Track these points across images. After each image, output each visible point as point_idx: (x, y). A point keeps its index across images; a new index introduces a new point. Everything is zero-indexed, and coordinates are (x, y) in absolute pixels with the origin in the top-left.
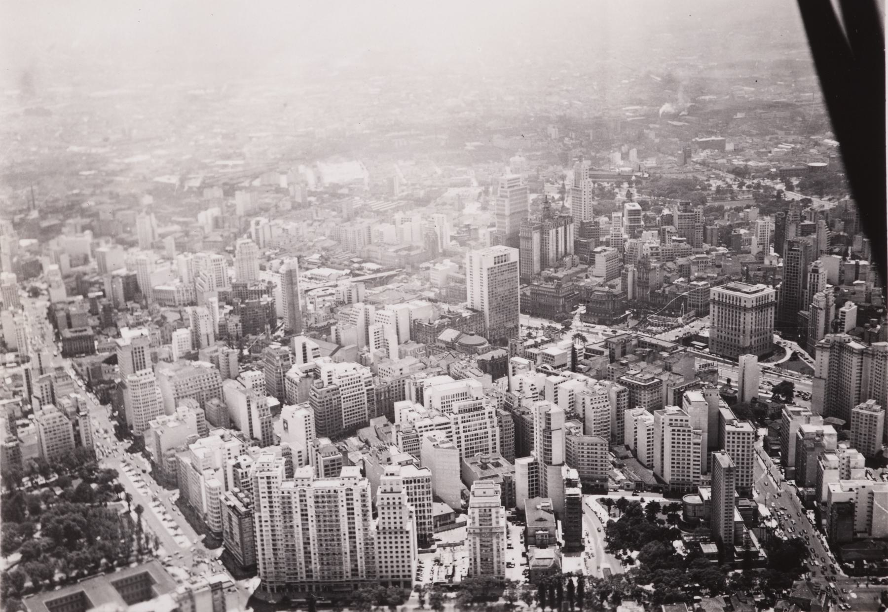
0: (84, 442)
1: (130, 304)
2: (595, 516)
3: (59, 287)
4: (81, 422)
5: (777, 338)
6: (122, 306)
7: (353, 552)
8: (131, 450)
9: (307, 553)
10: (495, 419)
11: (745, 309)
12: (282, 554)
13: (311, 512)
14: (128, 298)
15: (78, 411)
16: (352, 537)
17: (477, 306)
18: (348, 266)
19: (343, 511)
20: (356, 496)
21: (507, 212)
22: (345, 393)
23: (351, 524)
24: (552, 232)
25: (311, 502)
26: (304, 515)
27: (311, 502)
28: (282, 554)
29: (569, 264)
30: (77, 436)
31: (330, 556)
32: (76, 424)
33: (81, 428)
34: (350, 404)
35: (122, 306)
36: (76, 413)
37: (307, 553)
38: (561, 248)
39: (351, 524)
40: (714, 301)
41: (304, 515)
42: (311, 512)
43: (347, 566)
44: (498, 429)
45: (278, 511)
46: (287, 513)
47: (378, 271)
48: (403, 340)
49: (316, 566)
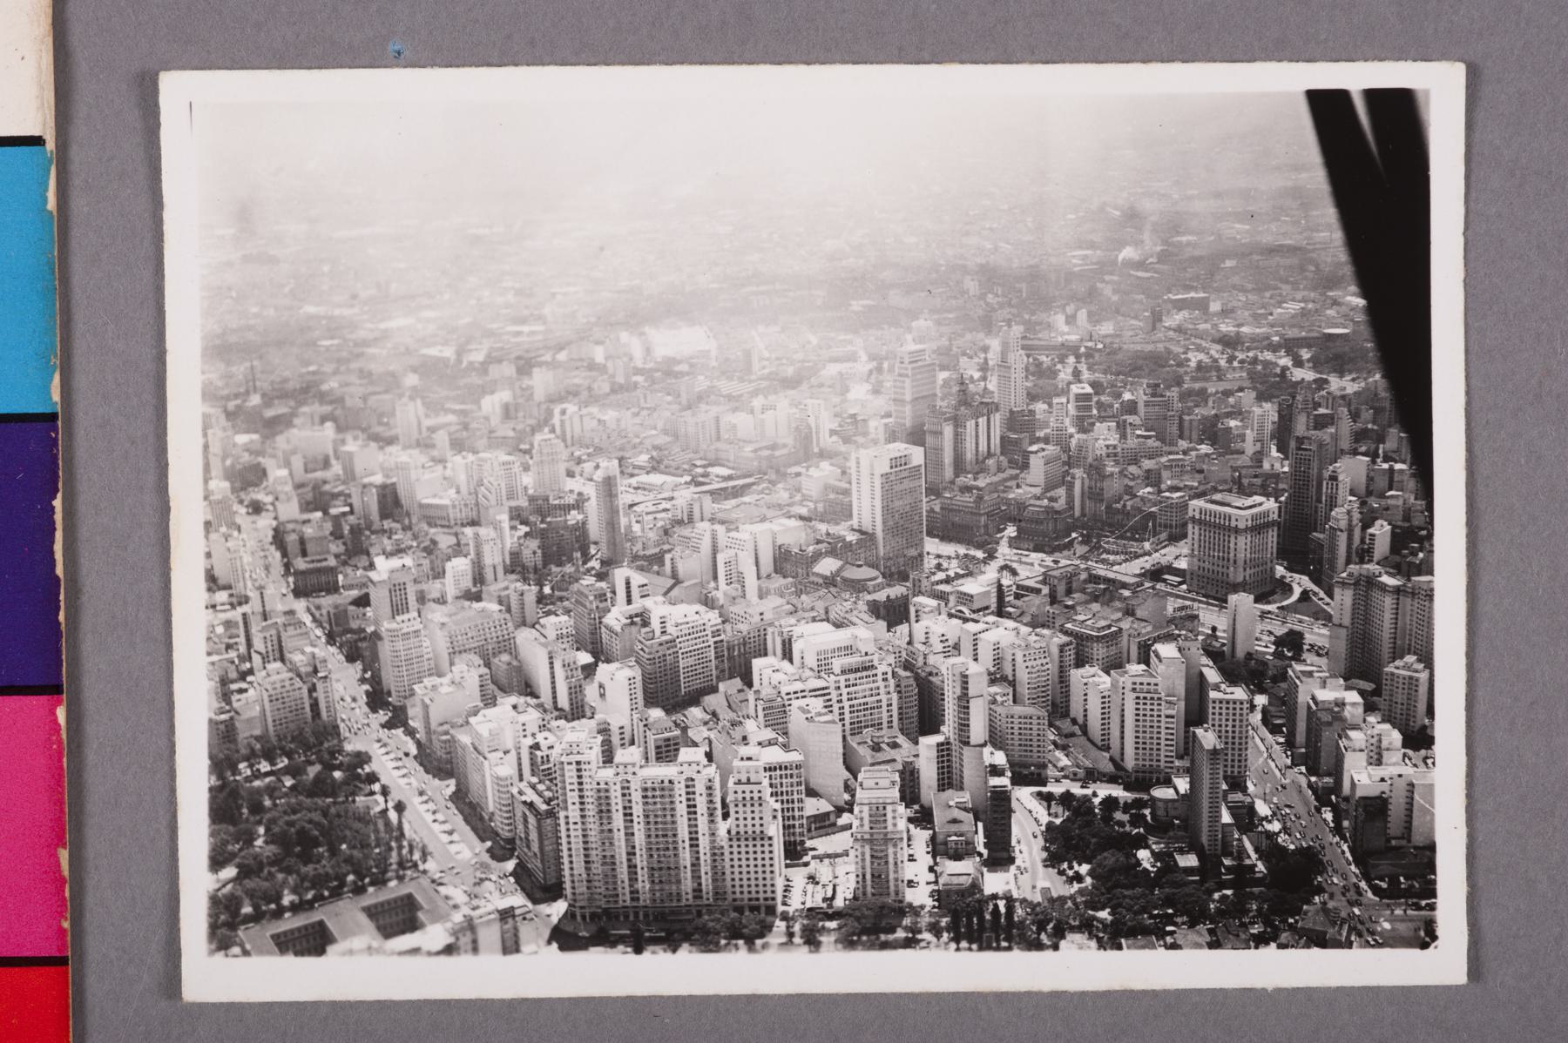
2: (1030, 816)
3: (289, 500)
4: (320, 686)
5: (1280, 570)
7: (695, 865)
8: (389, 725)
9: (632, 867)
10: (892, 682)
11: (1237, 531)
13: (637, 810)
14: (384, 515)
15: (316, 671)
17: (867, 527)
18: (688, 472)
19: (681, 809)
20: (700, 788)
21: (908, 397)
22: (685, 646)
23: (693, 826)
24: (970, 424)
25: (636, 797)
26: (628, 815)
27: (636, 797)
28: (597, 868)
29: (993, 469)
30: (315, 706)
31: (664, 871)
32: (313, 689)
33: (320, 694)
34: (691, 661)
35: (376, 526)
37: (632, 867)
38: (983, 447)
39: (693, 826)
40: (1193, 519)
41: (628, 815)
42: (637, 810)
43: (688, 885)
44: (895, 696)
45: (591, 810)
46: (604, 812)
47: (730, 478)
48: (764, 573)
49: (643, 884)
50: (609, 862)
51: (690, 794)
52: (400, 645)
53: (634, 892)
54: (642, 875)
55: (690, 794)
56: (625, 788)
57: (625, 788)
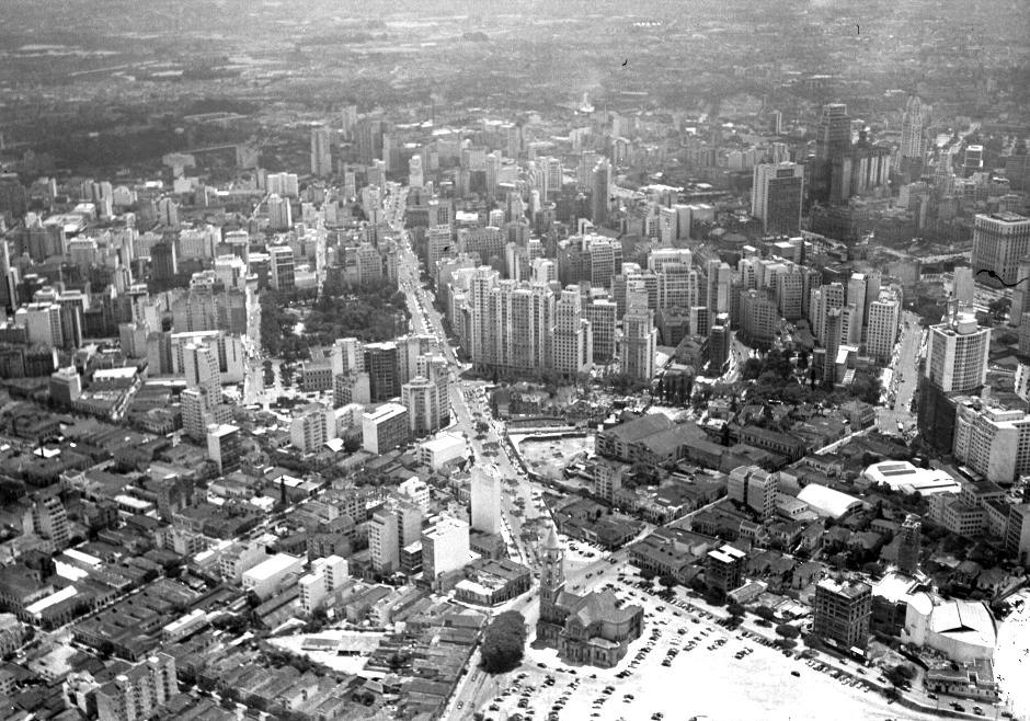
0: (390, 274)
1: (472, 195)
2: (738, 356)
3: (417, 174)
4: (389, 258)
5: (585, 95)
6: (466, 196)
7: (536, 346)
8: (425, 288)
9: (505, 343)
10: (696, 281)
11: (1001, 236)
12: (487, 343)
13: (509, 311)
14: (473, 189)
15: (389, 249)
16: (536, 335)
17: (759, 215)
18: (683, 185)
19: (532, 312)
20: (541, 302)
21: (826, 139)
22: (594, 260)
23: (536, 324)
24: (864, 161)
25: (509, 304)
26: (504, 314)
27: (509, 304)
28: (487, 343)
29: (878, 195)
30: (385, 270)
31: (520, 348)
32: (385, 260)
33: (388, 262)
34: (598, 269)
35: (466, 196)
36: (386, 254)
37: (505, 343)
38: (873, 178)
39: (536, 324)
40: (977, 228)
41: (504, 314)
42: (509, 311)
43: (532, 357)
44: (697, 290)
45: (486, 308)
46: (493, 310)
47: (707, 189)
48: (682, 235)
49: (510, 354)
50: (493, 338)
51: (536, 305)
52: (436, 242)
53: (505, 358)
54: (509, 348)
55: (536, 305)
56: (504, 298)
57: (504, 298)
